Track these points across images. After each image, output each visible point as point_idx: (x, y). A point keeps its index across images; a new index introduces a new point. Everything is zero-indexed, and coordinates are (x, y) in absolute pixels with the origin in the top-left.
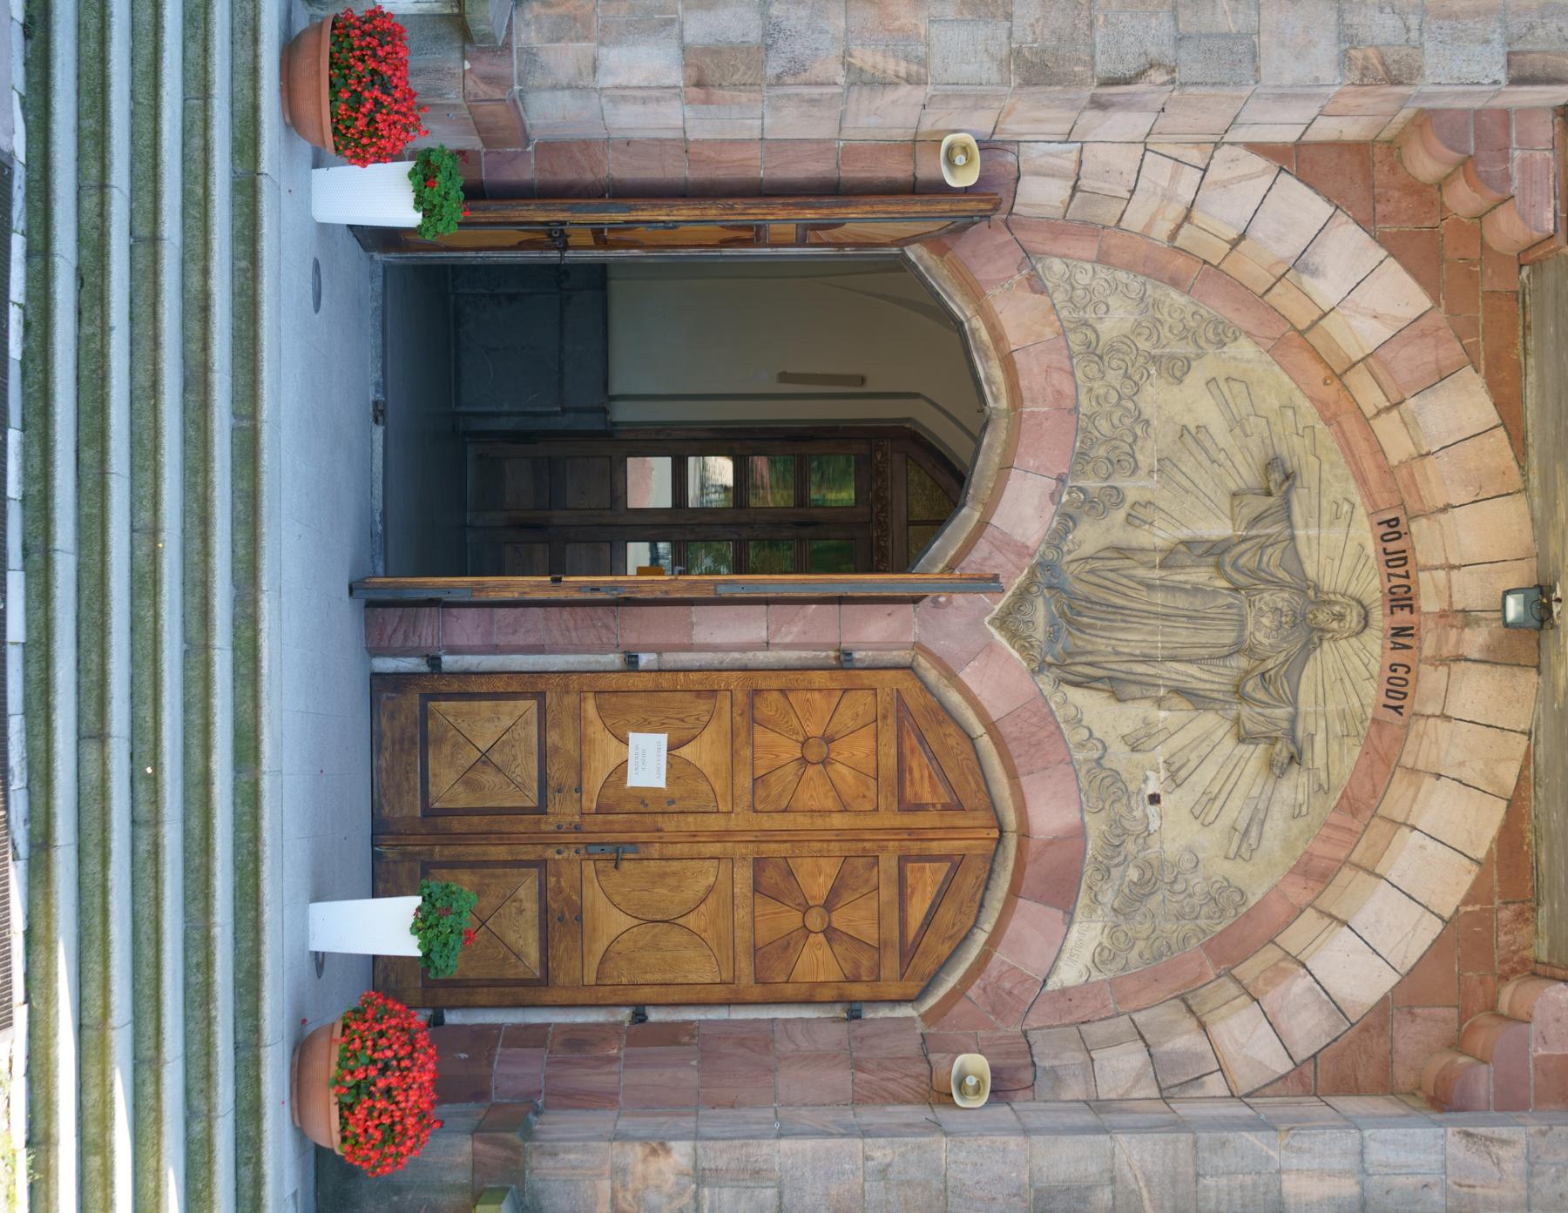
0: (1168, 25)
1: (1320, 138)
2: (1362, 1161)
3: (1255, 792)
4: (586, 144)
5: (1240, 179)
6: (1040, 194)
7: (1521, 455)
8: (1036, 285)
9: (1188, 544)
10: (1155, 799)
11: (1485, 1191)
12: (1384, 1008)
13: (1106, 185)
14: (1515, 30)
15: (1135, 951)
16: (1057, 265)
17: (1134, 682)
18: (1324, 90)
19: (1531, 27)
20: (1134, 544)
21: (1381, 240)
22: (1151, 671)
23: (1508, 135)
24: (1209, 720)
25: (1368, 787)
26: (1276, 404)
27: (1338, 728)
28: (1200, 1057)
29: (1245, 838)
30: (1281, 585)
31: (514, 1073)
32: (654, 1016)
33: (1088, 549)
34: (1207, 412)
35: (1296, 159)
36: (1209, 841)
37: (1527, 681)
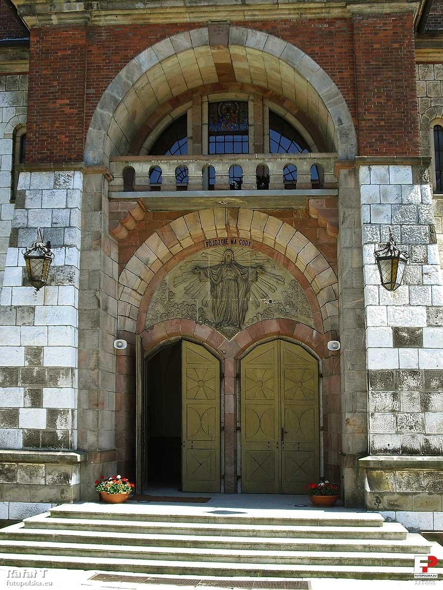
0: (86, 291)
1: (117, 258)
2: (349, 248)
3: (269, 277)
4: (116, 435)
5: (126, 277)
6: (130, 325)
7: (191, 211)
8: (152, 328)
9: (212, 292)
10: (270, 301)
11: (356, 218)
12: (318, 246)
13: (128, 310)
14: (89, 209)
15: (306, 306)
16: (148, 322)
17: (243, 306)
18: (102, 255)
19: (89, 205)
20: (212, 305)
21: (141, 244)
22: (241, 301)
23: (115, 212)
24: (253, 288)
25: (268, 250)
26: (180, 271)
27: (254, 257)
28: (328, 289)
29: (280, 280)
30: (221, 270)
31: (333, 460)
32: (322, 425)
33: (213, 316)
34: (181, 287)
35: (122, 264)
36: (280, 289)
37: (241, 211)
